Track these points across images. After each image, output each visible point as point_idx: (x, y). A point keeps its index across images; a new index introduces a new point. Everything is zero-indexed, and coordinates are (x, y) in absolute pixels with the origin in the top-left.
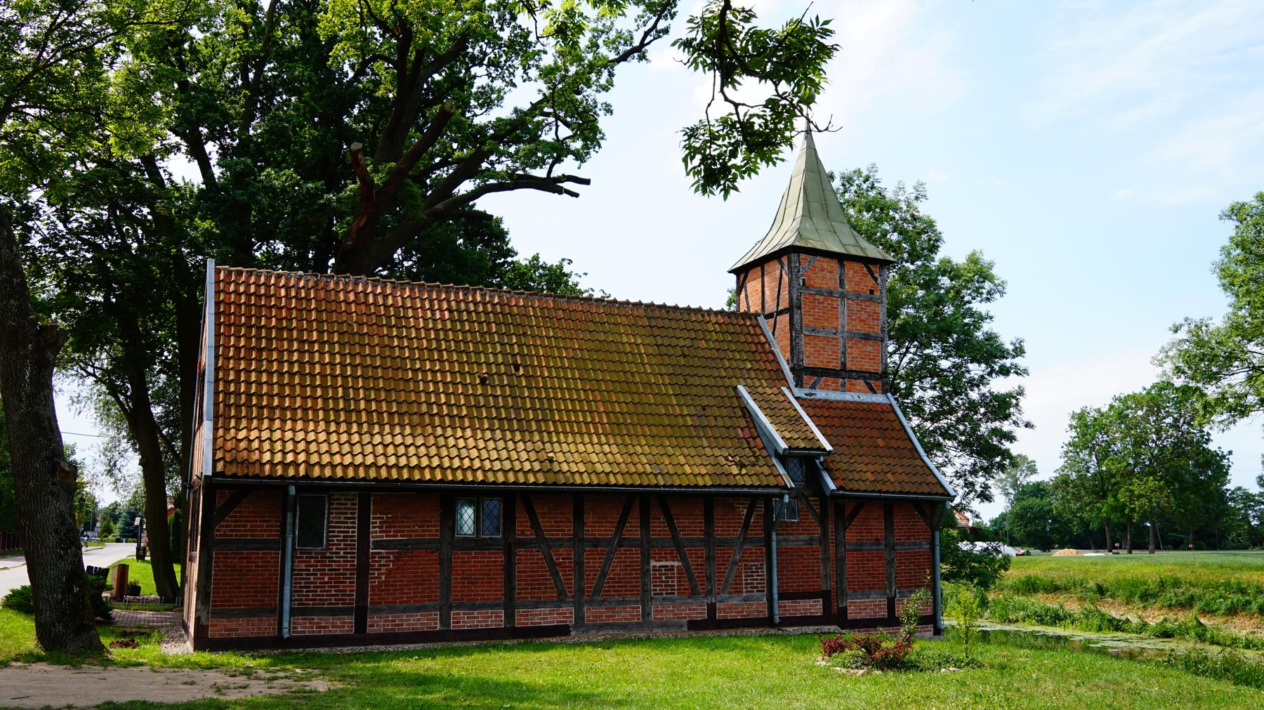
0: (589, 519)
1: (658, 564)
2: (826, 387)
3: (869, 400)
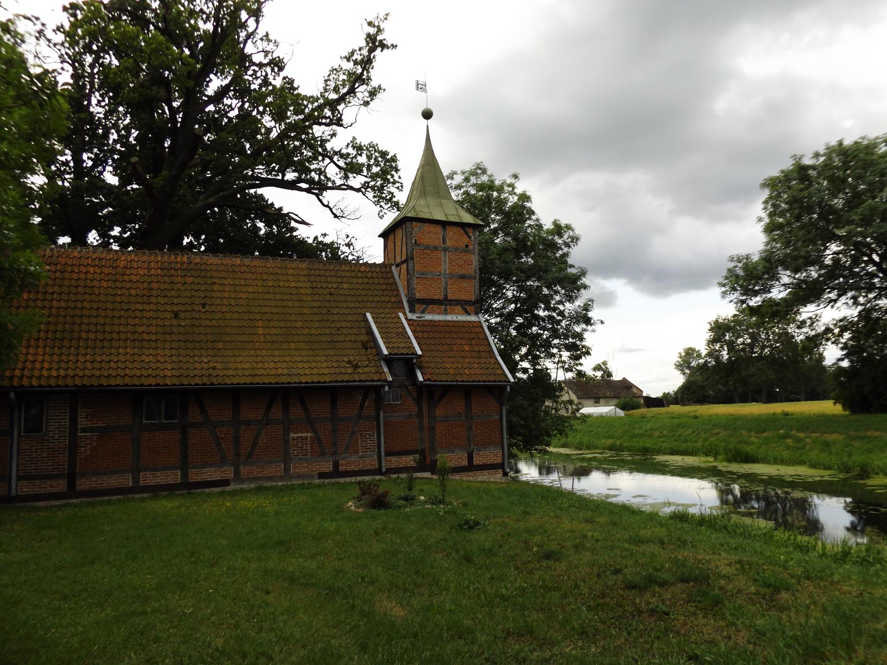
1: (296, 435)
3: (464, 319)
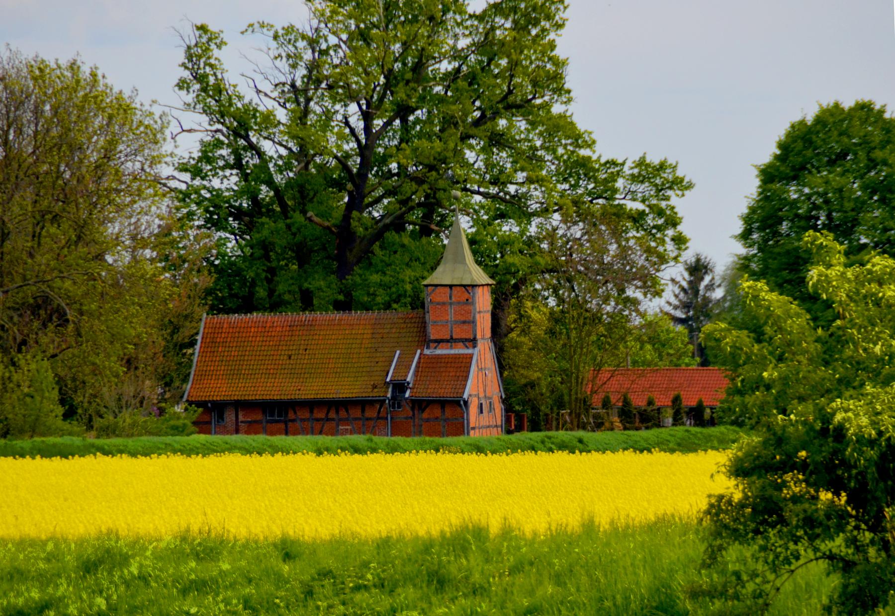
0: (315, 411)
2: (442, 348)
